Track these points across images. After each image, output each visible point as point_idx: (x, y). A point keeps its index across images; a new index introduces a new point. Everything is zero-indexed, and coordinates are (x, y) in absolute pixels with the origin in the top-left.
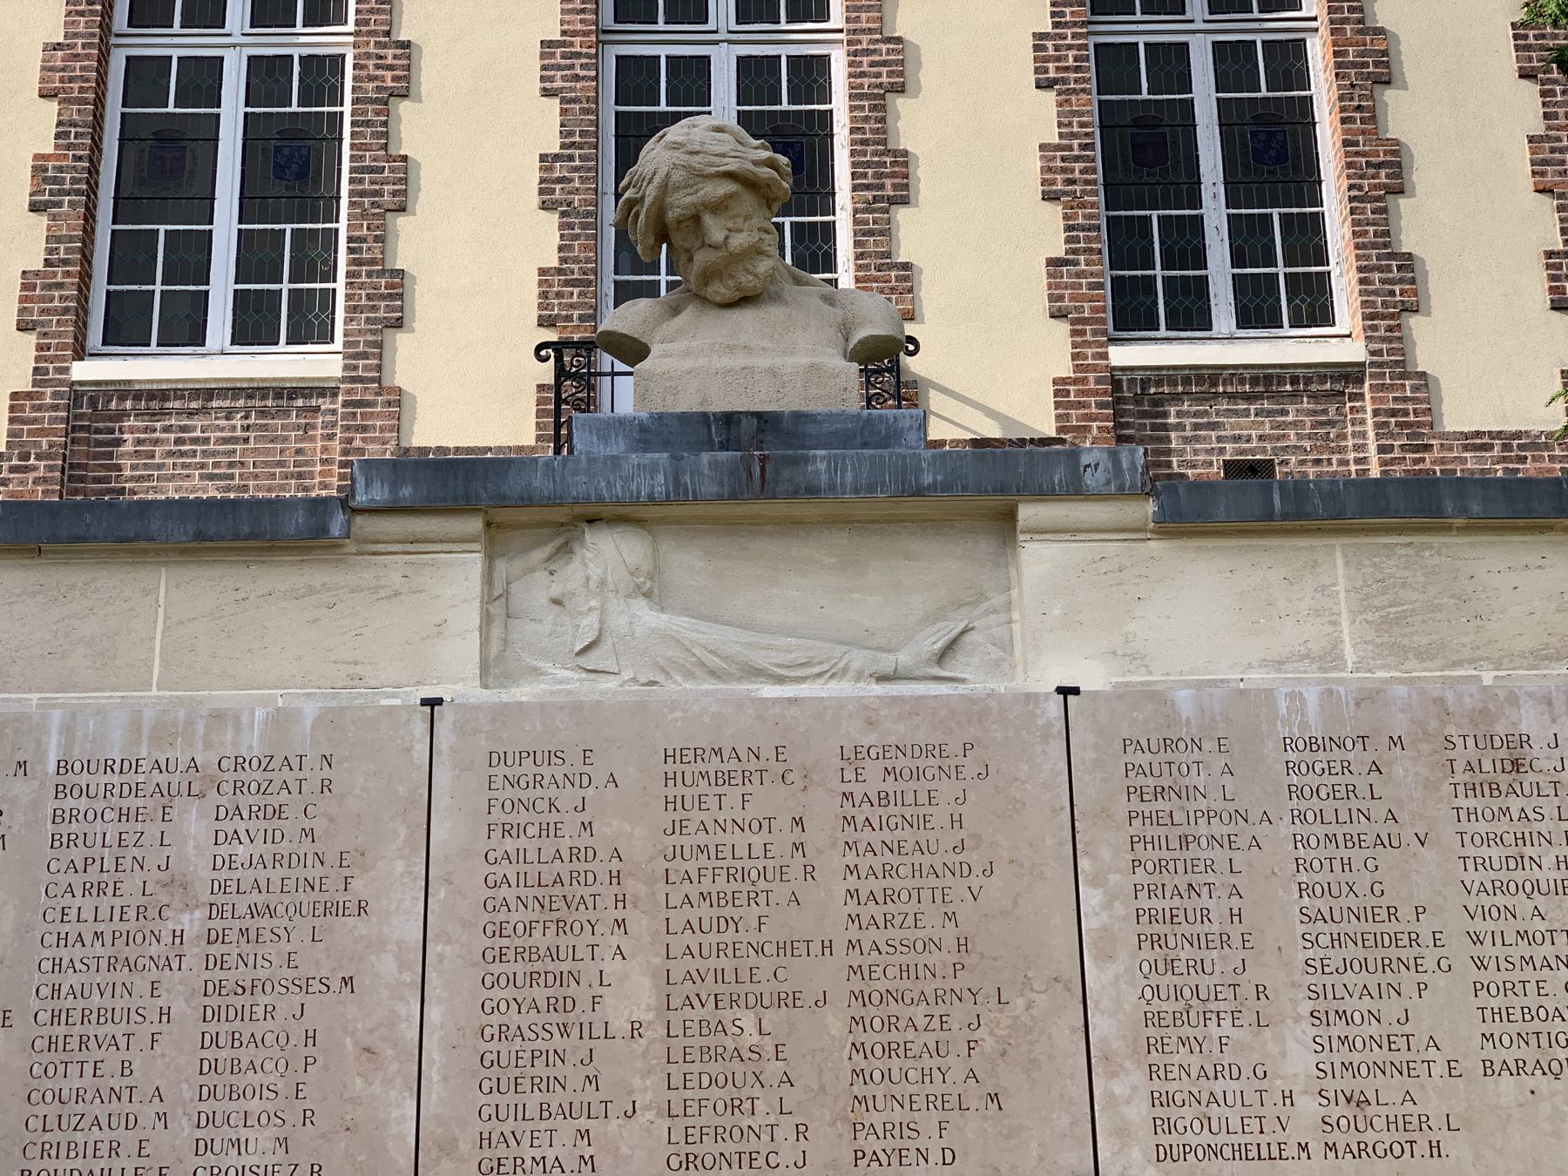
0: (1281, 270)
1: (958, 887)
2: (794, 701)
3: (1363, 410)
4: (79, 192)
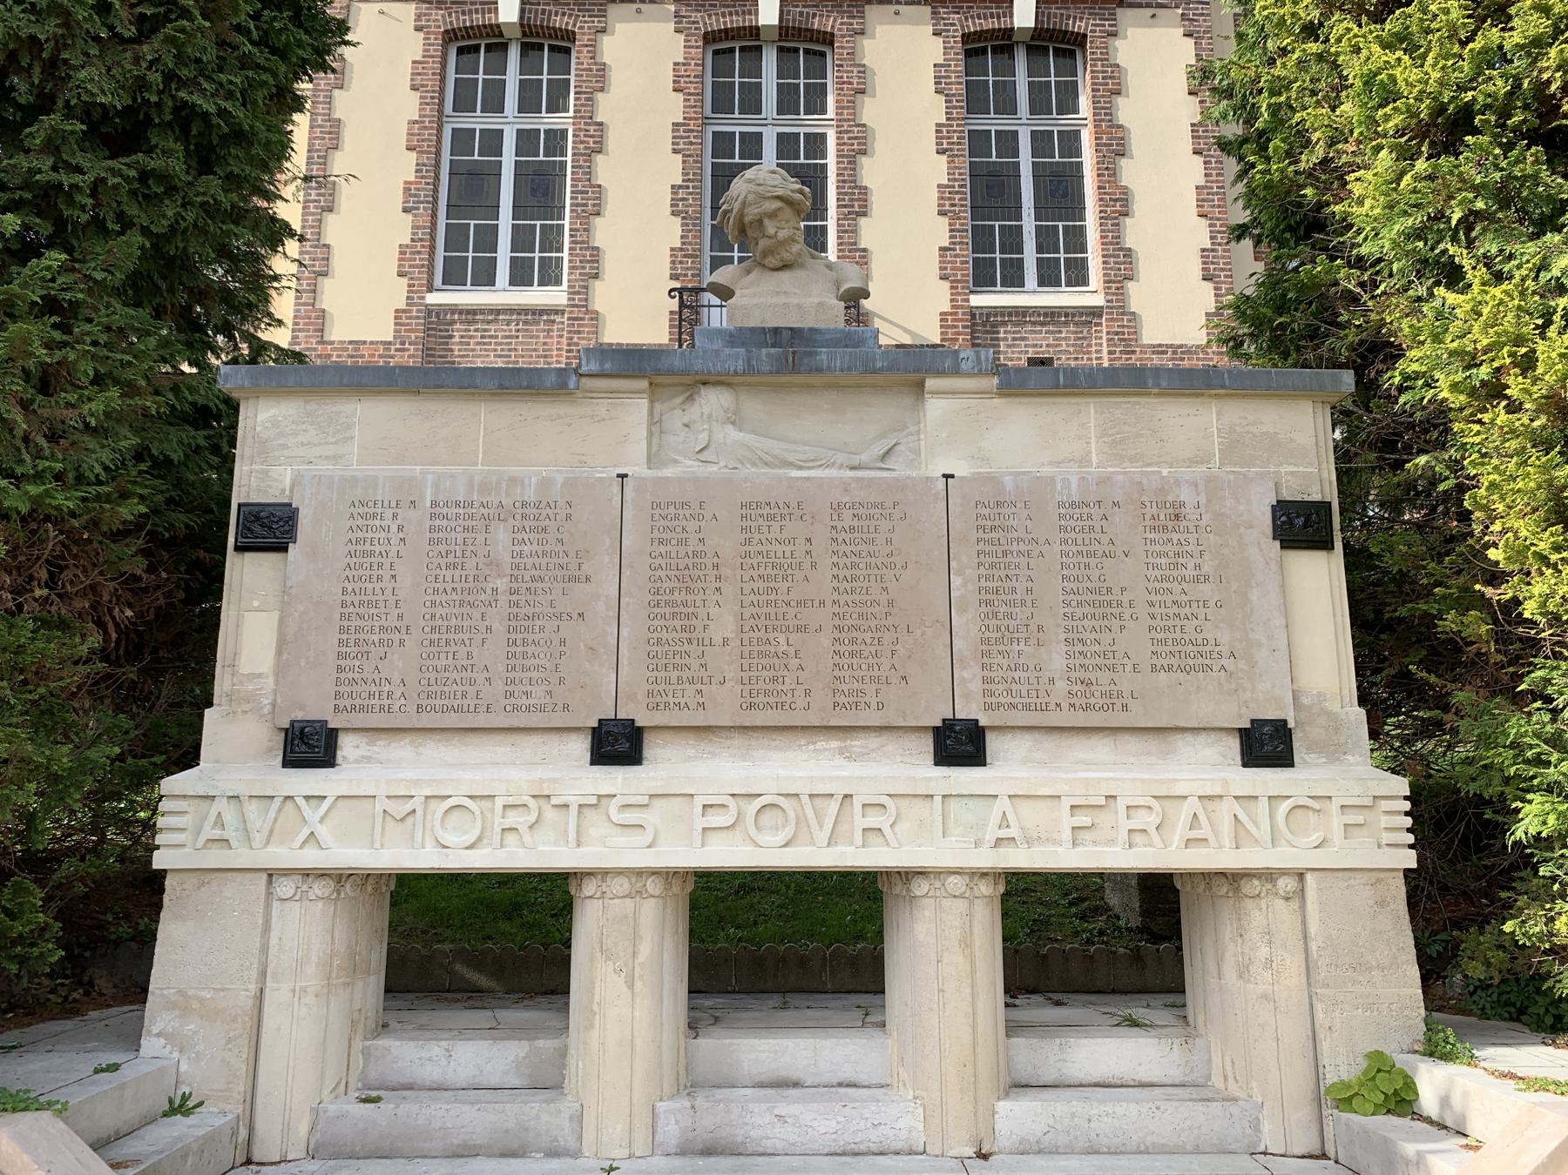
0: (1062, 256)
1: (889, 574)
2: (807, 479)
3: (1101, 331)
4: (428, 202)
